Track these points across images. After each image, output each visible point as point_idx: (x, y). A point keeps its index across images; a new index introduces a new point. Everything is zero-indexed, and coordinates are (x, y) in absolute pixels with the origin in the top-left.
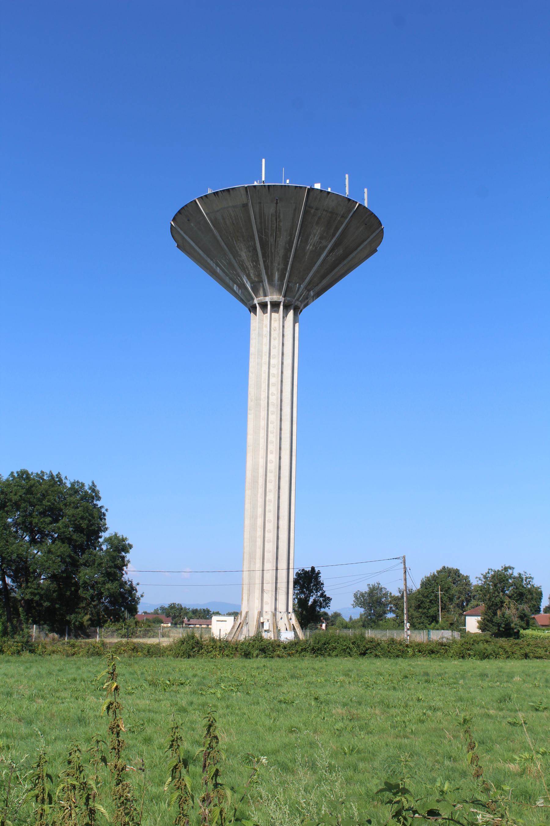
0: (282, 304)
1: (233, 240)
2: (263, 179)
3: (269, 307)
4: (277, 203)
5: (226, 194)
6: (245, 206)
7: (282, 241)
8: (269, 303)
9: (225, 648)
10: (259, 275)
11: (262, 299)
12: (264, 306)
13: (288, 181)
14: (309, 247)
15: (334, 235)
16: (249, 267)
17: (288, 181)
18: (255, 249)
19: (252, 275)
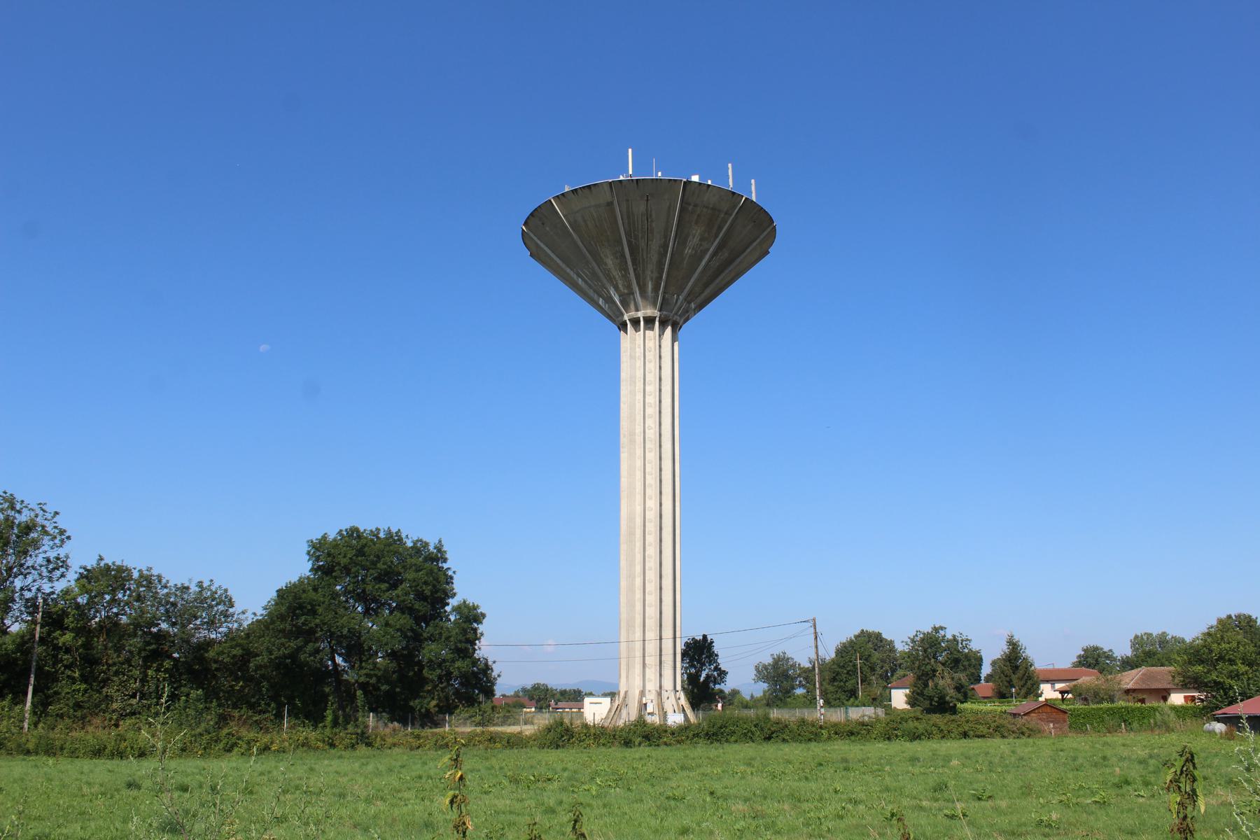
5: (587, 191)
6: (610, 204)
7: (655, 244)
9: (601, 736)
10: (629, 286)
11: (633, 314)
12: (635, 322)
14: (688, 251)
15: (716, 237)
18: (623, 256)
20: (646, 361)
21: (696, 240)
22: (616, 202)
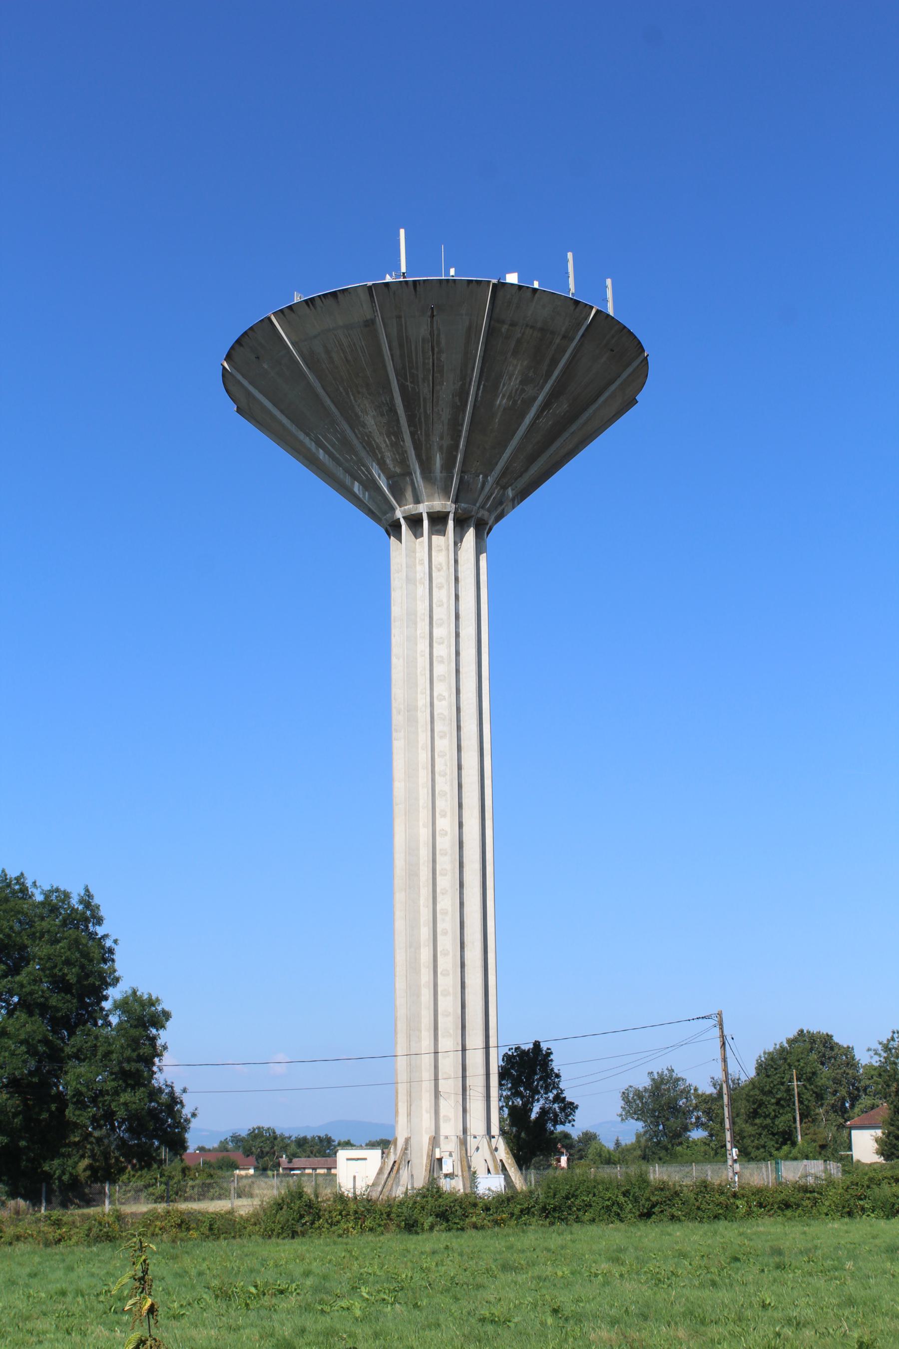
0: (451, 516)
1: (347, 394)
2: (403, 269)
3: (426, 523)
4: (432, 316)
5: (330, 301)
6: (369, 324)
7: (447, 390)
8: (425, 517)
10: (403, 461)
11: (411, 508)
12: (415, 522)
13: (452, 272)
14: (501, 401)
16: (383, 446)
17: (452, 272)
18: (392, 410)
19: (388, 461)
20: (432, 582)
21: (514, 383)
22: (379, 320)
